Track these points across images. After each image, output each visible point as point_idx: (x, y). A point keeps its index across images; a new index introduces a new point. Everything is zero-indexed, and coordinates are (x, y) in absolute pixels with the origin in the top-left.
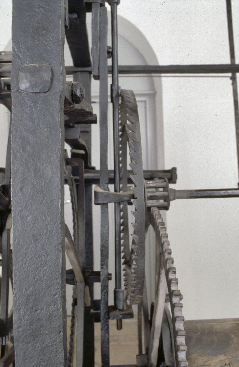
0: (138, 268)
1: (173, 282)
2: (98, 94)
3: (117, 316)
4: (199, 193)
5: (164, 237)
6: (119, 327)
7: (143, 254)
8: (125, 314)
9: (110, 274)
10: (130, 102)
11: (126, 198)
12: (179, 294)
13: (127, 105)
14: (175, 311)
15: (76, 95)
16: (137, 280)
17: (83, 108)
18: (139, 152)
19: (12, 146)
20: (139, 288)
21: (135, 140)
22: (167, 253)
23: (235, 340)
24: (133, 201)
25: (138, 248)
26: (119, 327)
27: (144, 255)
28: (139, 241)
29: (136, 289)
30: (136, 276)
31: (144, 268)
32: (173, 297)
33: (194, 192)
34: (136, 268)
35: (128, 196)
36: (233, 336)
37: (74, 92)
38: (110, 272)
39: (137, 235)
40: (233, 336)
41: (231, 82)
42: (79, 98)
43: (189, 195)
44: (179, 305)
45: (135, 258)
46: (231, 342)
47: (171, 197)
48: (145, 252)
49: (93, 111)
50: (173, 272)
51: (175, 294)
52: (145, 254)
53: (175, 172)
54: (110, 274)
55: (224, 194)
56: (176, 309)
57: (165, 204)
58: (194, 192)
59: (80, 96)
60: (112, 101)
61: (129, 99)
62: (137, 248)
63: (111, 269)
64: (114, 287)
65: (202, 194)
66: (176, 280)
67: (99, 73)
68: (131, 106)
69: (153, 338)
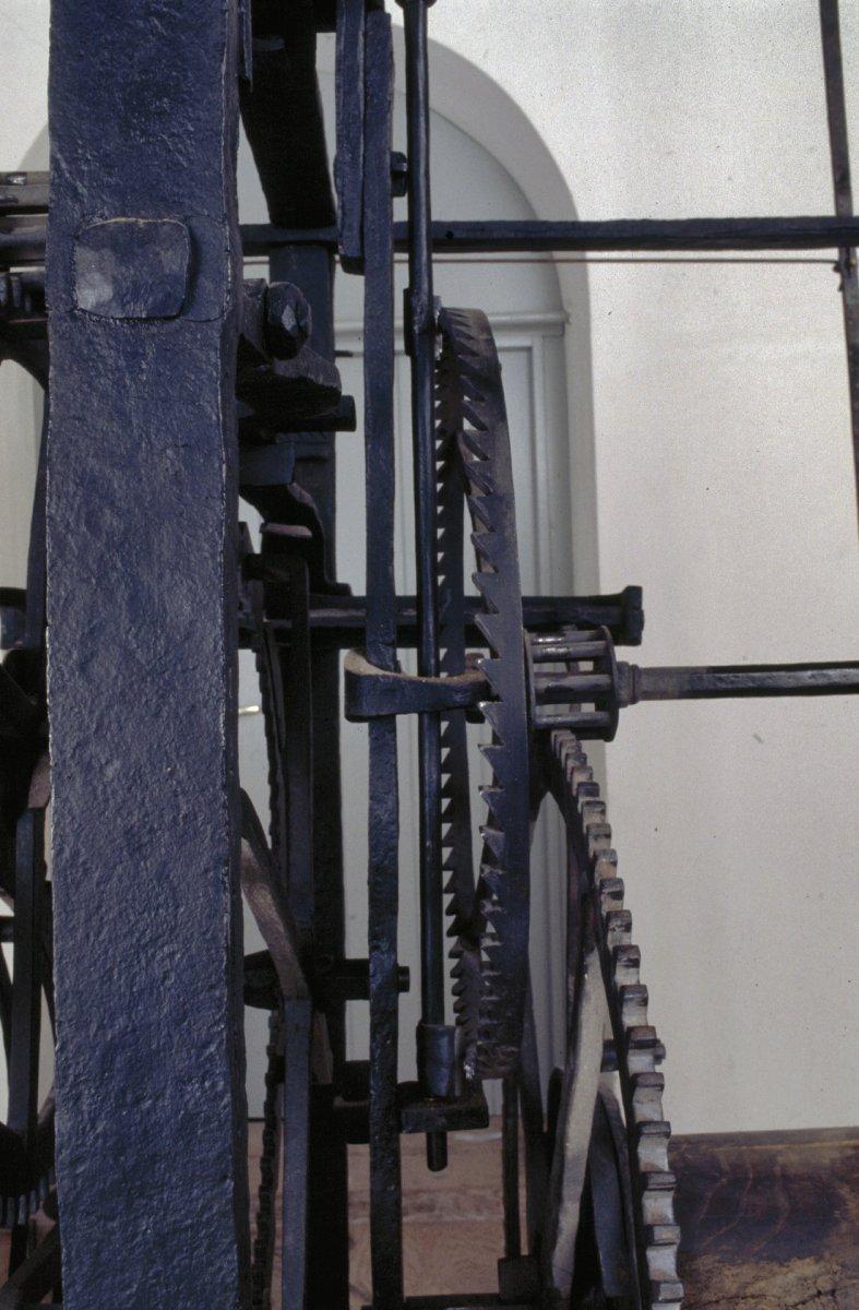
1: (631, 999)
4: (720, 679)
6: (437, 1158)
9: (405, 971)
10: (474, 354)
18: (506, 534)
19: (50, 510)
21: (492, 490)
24: (485, 708)
26: (437, 1158)
29: (495, 1022)
30: (495, 976)
32: (631, 1052)
40: (844, 1191)
41: (837, 278)
50: (630, 960)
54: (405, 971)
55: (812, 682)
56: (641, 1094)
61: (471, 341)
63: (408, 951)
65: (732, 682)
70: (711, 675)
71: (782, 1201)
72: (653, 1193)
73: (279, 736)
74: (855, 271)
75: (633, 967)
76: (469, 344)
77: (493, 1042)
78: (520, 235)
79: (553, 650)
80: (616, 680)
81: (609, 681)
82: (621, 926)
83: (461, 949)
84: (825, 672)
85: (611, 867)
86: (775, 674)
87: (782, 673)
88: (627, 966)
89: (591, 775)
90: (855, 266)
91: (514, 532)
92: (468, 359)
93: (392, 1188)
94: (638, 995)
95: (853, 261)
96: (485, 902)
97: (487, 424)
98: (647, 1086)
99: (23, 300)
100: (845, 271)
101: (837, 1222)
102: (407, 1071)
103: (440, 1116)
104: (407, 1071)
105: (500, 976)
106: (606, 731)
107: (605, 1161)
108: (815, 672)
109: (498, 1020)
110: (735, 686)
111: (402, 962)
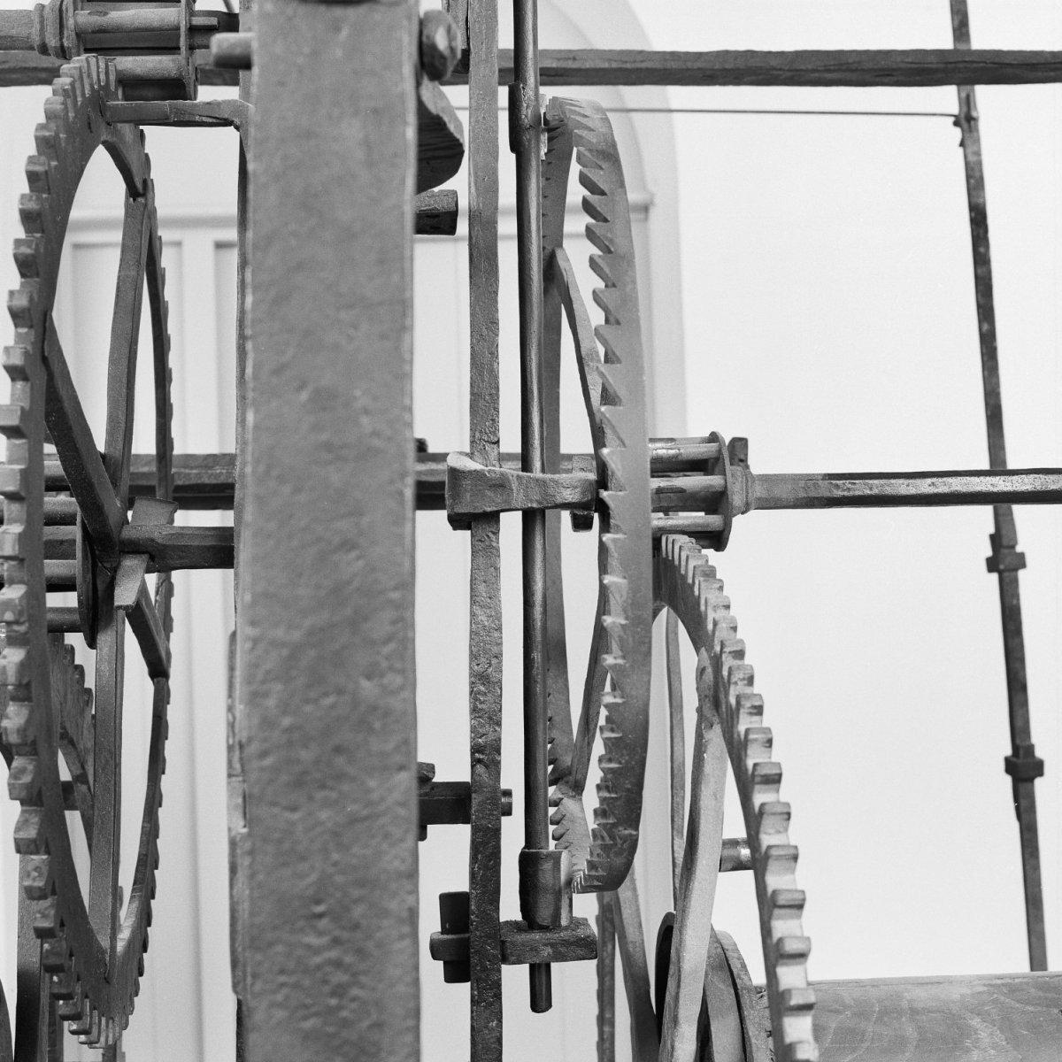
0: (624, 702)
1: (756, 740)
2: (466, 104)
3: (534, 949)
4: (837, 486)
5: (715, 608)
6: (540, 1000)
7: (644, 649)
8: (566, 943)
9: (508, 793)
10: (591, 130)
11: (569, 491)
12: (776, 774)
13: (581, 137)
14: (765, 833)
15: (434, 47)
16: (622, 755)
17: (441, 115)
18: (628, 290)
19: (251, 167)
20: (628, 790)
21: (612, 249)
22: (730, 653)
23: (983, 1035)
24: (609, 454)
25: (626, 625)
26: (540, 1000)
27: (648, 653)
28: (630, 601)
29: (613, 795)
30: (615, 738)
31: (647, 705)
32: (757, 787)
33: (820, 482)
34: (616, 704)
35: (576, 487)
36: (975, 1022)
37: (428, 37)
38: (504, 785)
39: (625, 578)
40: (975, 1022)
41: (957, 134)
42: (442, 57)
43: (802, 494)
44: (779, 809)
45: (616, 665)
46: (968, 1043)
47: (737, 499)
48: (650, 642)
49: (21, 902)
50: (754, 707)
51: (762, 776)
52: (650, 648)
53: (742, 457)
54: (508, 793)
55: (932, 490)
56: (768, 824)
57: (714, 521)
58: (820, 482)
59: (446, 53)
60: (516, 145)
61: (586, 119)
62: (621, 625)
63: (512, 776)
64: (521, 843)
65: (849, 489)
66: (765, 733)
67: (468, 44)
68: (594, 141)
69: (675, 1021)
70: (827, 482)
71: (910, 1031)
72: (782, 911)
73: (538, 176)
74: (976, 126)
75: (756, 714)
76: (584, 121)
77: (611, 821)
78: (614, 65)
79: (664, 451)
80: (730, 479)
81: (722, 482)
82: (744, 679)
83: (561, 796)
84: (945, 479)
85: (732, 632)
86: (893, 481)
87: (901, 481)
88: (751, 714)
89: (707, 561)
90: (975, 119)
91: (634, 289)
92: (584, 133)
93: (494, 1024)
94: (763, 736)
95: (974, 114)
96: (605, 656)
97: (606, 190)
98: (774, 814)
99: (116, 90)
100: (965, 125)
101: (968, 1051)
102: (510, 908)
103: (546, 945)
104: (510, 908)
105: (621, 737)
106: (716, 539)
107: (722, 986)
108: (934, 480)
109: (616, 793)
110: (851, 493)
111: (504, 784)
